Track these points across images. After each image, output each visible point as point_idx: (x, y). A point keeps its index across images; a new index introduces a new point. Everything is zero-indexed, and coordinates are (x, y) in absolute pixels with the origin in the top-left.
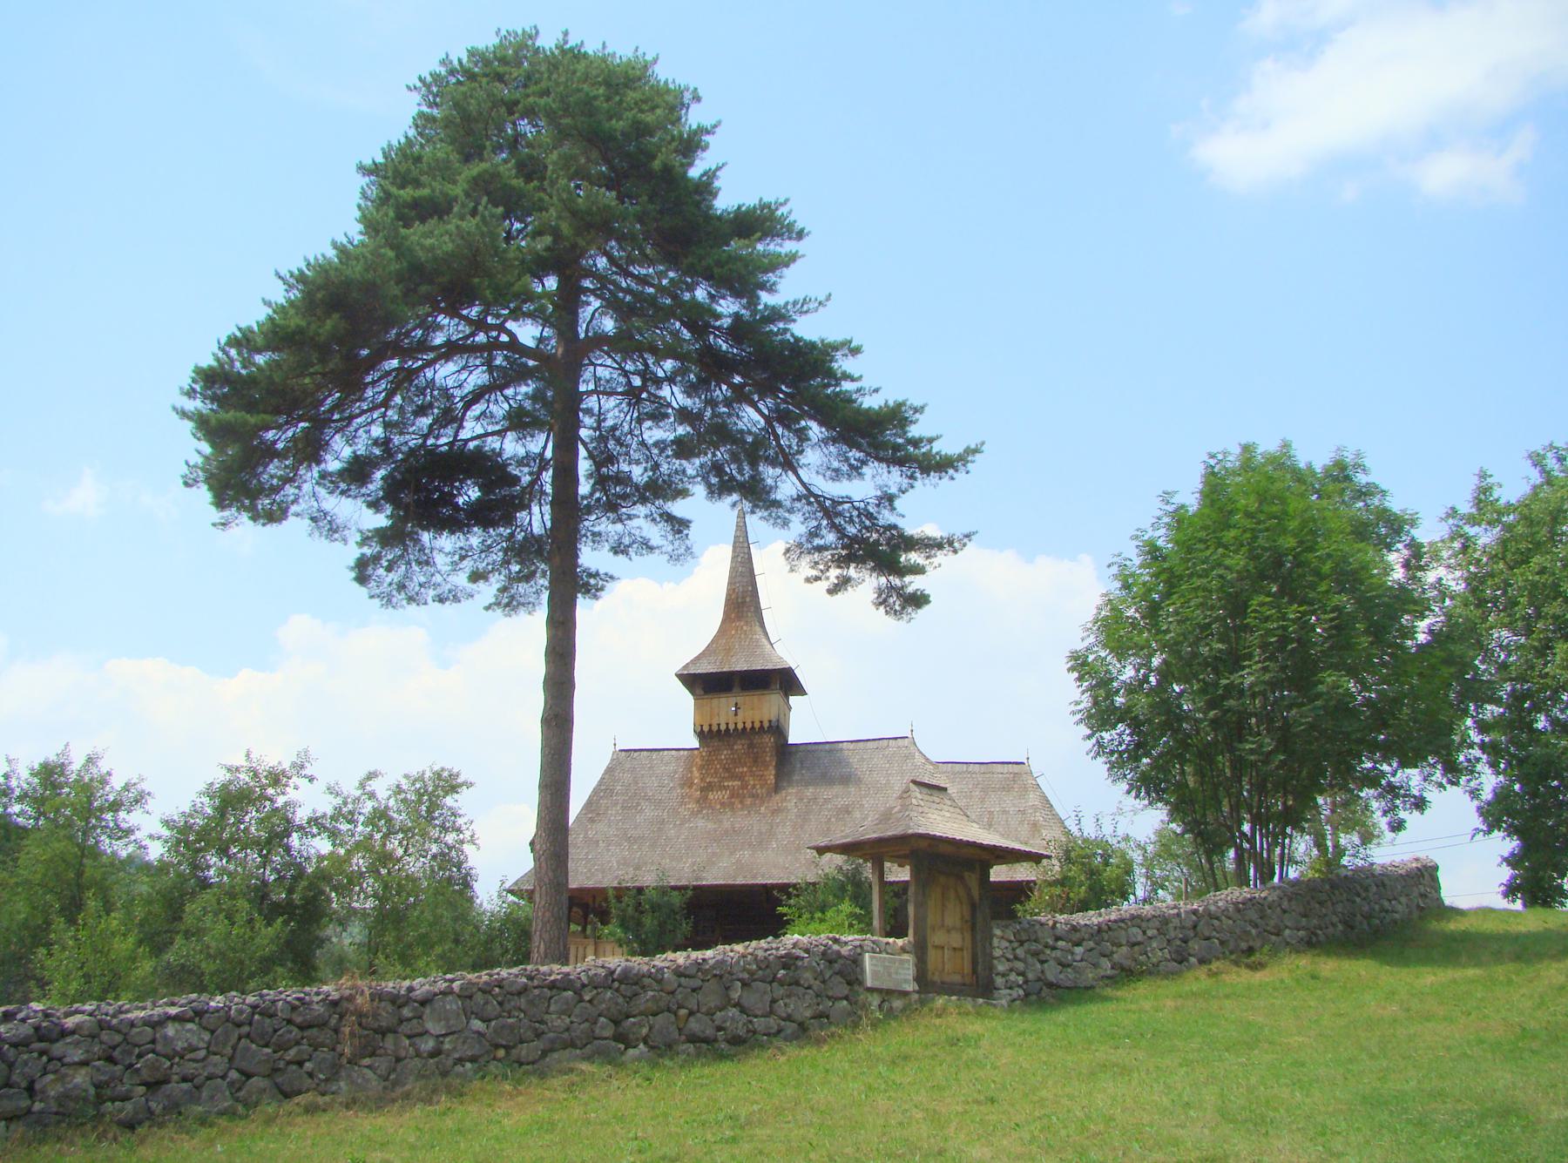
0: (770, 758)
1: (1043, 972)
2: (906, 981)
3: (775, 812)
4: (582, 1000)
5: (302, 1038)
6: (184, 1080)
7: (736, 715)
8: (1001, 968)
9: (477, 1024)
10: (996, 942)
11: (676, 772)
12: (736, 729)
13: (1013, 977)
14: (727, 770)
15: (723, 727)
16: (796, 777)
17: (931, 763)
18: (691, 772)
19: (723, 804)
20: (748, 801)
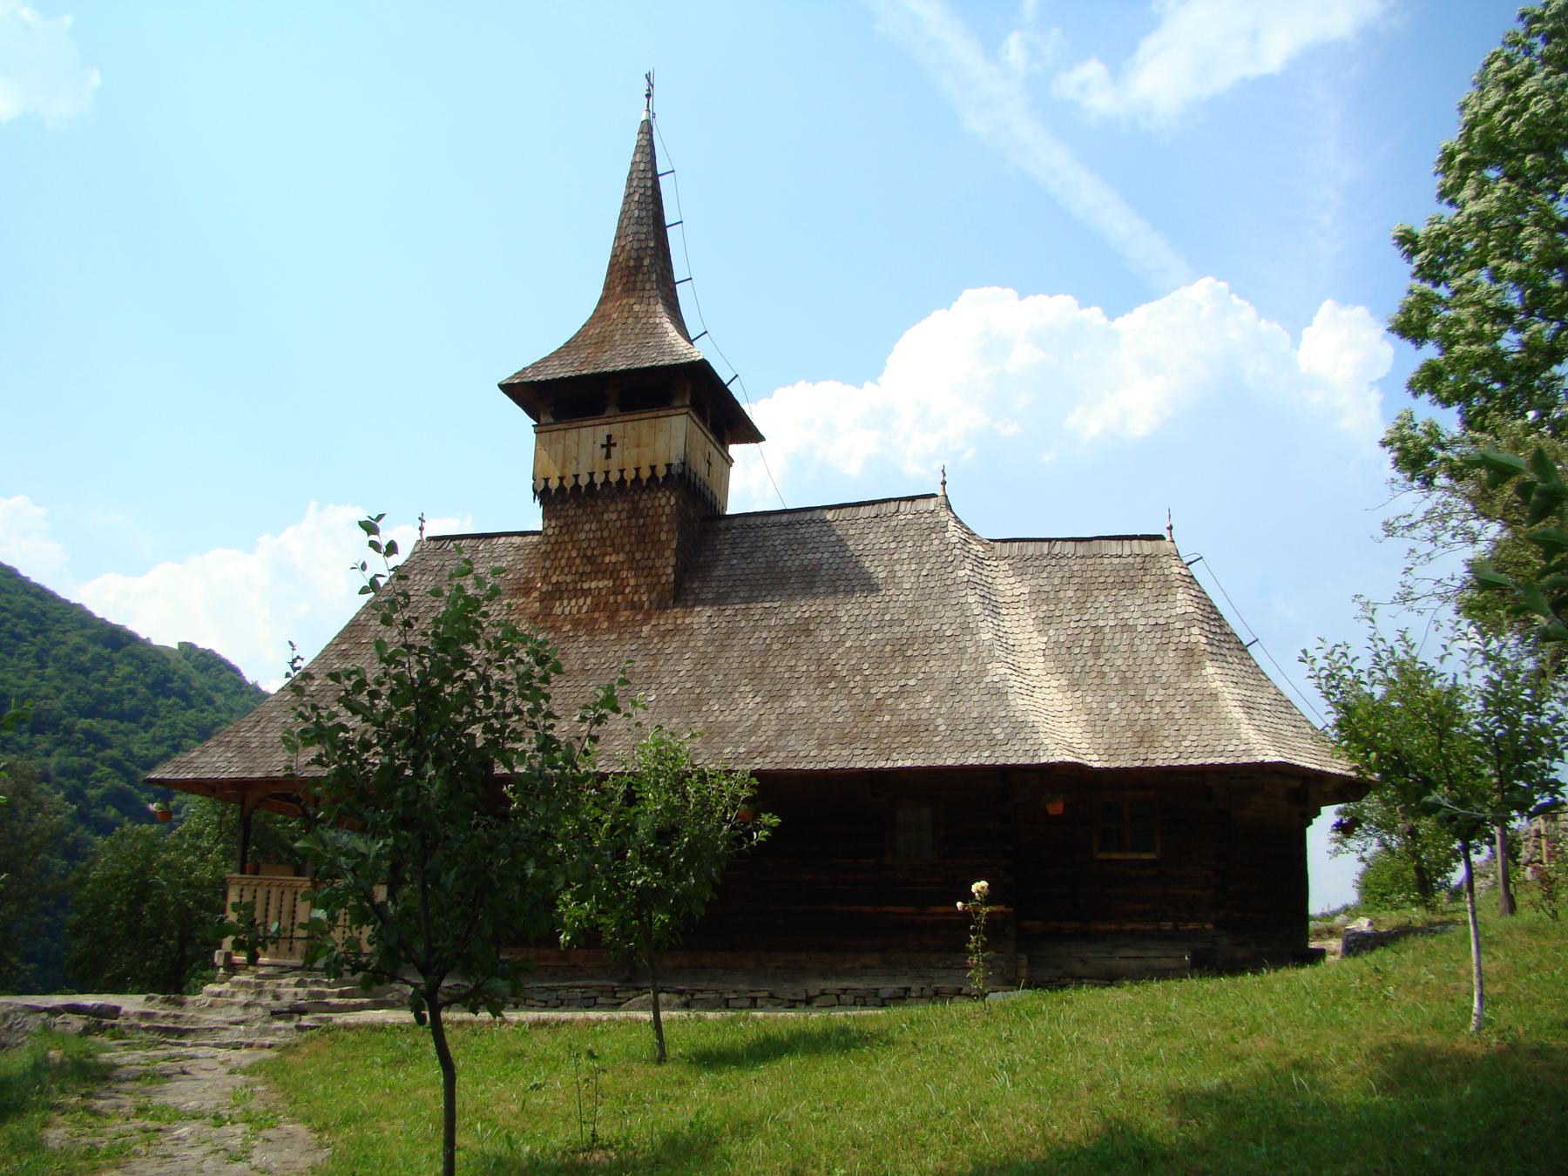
7: (608, 456)
14: (590, 560)
17: (980, 542)
19: (576, 623)
20: (624, 615)
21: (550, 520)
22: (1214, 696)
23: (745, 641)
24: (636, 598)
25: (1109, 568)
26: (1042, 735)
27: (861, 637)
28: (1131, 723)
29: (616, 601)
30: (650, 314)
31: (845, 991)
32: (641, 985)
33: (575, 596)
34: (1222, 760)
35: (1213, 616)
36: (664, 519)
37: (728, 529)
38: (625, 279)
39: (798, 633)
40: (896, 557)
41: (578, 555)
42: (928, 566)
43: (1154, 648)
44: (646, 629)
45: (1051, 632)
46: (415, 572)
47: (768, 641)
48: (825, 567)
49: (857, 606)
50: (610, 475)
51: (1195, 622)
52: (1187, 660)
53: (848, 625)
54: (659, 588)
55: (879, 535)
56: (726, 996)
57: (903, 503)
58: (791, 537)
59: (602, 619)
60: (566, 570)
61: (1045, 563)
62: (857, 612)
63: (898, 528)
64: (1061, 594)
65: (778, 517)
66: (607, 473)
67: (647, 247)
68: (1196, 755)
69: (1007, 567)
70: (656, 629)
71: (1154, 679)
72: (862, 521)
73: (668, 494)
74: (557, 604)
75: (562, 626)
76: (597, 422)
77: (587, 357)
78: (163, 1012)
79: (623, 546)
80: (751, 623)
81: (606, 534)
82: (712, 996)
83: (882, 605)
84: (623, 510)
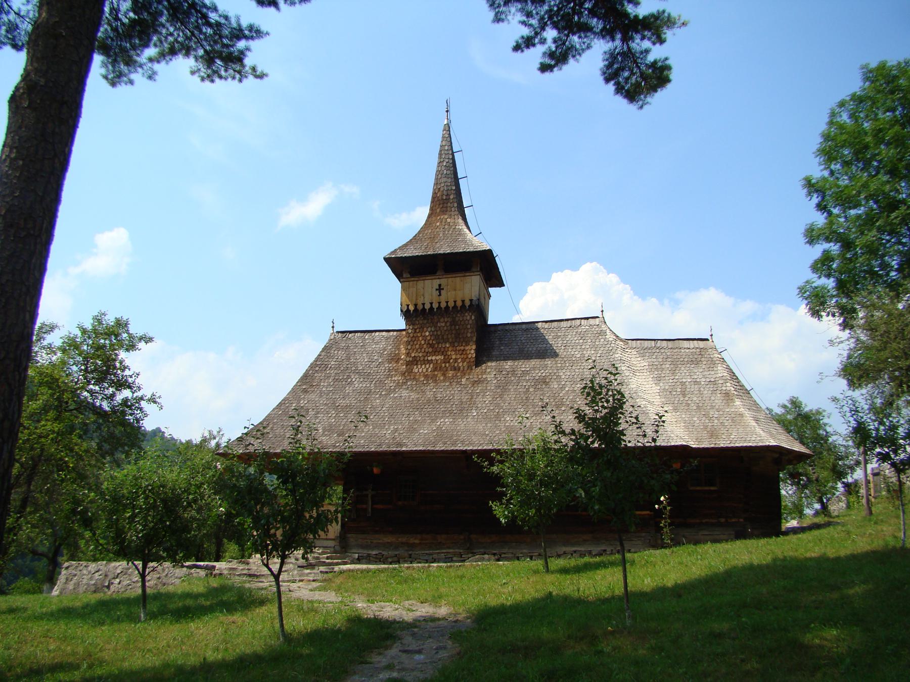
0: (471, 334)
3: (476, 383)
11: (385, 350)
12: (439, 308)
14: (431, 346)
15: (427, 307)
16: (495, 353)
17: (621, 340)
18: (399, 349)
19: (426, 376)
20: (451, 374)
21: (409, 325)
22: (741, 415)
23: (515, 387)
24: (456, 365)
25: (684, 354)
26: (669, 433)
27: (573, 386)
28: (706, 427)
29: (445, 366)
30: (455, 224)
31: (575, 552)
32: (475, 551)
33: (424, 363)
34: (750, 444)
35: (735, 377)
36: (469, 326)
37: (495, 331)
38: (441, 206)
39: (541, 383)
40: (583, 347)
41: (425, 343)
42: (600, 352)
43: (710, 392)
44: (464, 380)
45: (661, 384)
46: (334, 349)
47: (527, 387)
48: (549, 351)
49: (568, 371)
50: (441, 304)
51: (728, 381)
52: (727, 398)
53: (565, 380)
54: (468, 360)
55: (574, 336)
56: (517, 555)
57: (582, 320)
58: (529, 336)
59: (439, 375)
60: (419, 350)
61: (654, 351)
62: (569, 374)
63: (582, 333)
64: (663, 366)
65: (527, 325)
66: (439, 303)
67: (451, 190)
68: (738, 442)
69: (636, 353)
70: (468, 380)
71: (712, 407)
72: (563, 329)
73: (470, 314)
74: (415, 367)
75: (419, 378)
76: (433, 277)
77: (428, 245)
78: (241, 568)
79: (448, 339)
80: (517, 378)
81: (439, 333)
82: (510, 555)
83: (581, 370)
84: (448, 321)
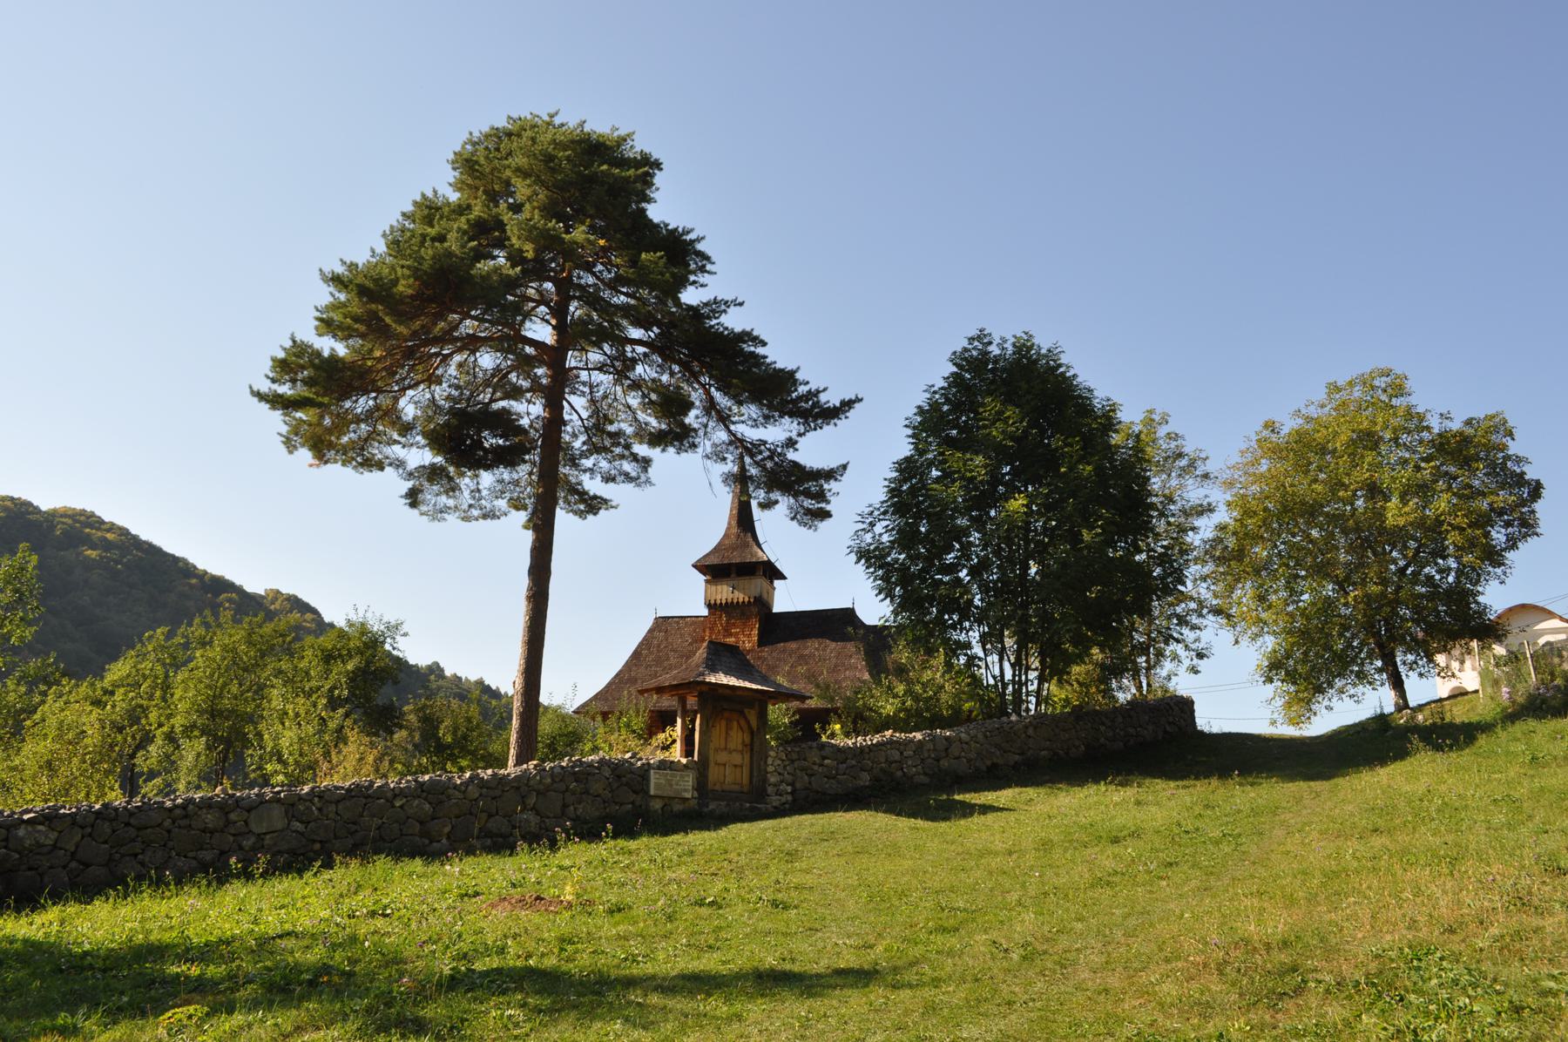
1: (810, 783)
2: (686, 790)
4: (393, 806)
5: (137, 836)
6: (30, 869)
8: (773, 780)
9: (297, 825)
10: (770, 761)
13: (783, 786)
